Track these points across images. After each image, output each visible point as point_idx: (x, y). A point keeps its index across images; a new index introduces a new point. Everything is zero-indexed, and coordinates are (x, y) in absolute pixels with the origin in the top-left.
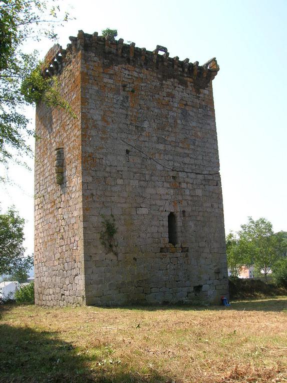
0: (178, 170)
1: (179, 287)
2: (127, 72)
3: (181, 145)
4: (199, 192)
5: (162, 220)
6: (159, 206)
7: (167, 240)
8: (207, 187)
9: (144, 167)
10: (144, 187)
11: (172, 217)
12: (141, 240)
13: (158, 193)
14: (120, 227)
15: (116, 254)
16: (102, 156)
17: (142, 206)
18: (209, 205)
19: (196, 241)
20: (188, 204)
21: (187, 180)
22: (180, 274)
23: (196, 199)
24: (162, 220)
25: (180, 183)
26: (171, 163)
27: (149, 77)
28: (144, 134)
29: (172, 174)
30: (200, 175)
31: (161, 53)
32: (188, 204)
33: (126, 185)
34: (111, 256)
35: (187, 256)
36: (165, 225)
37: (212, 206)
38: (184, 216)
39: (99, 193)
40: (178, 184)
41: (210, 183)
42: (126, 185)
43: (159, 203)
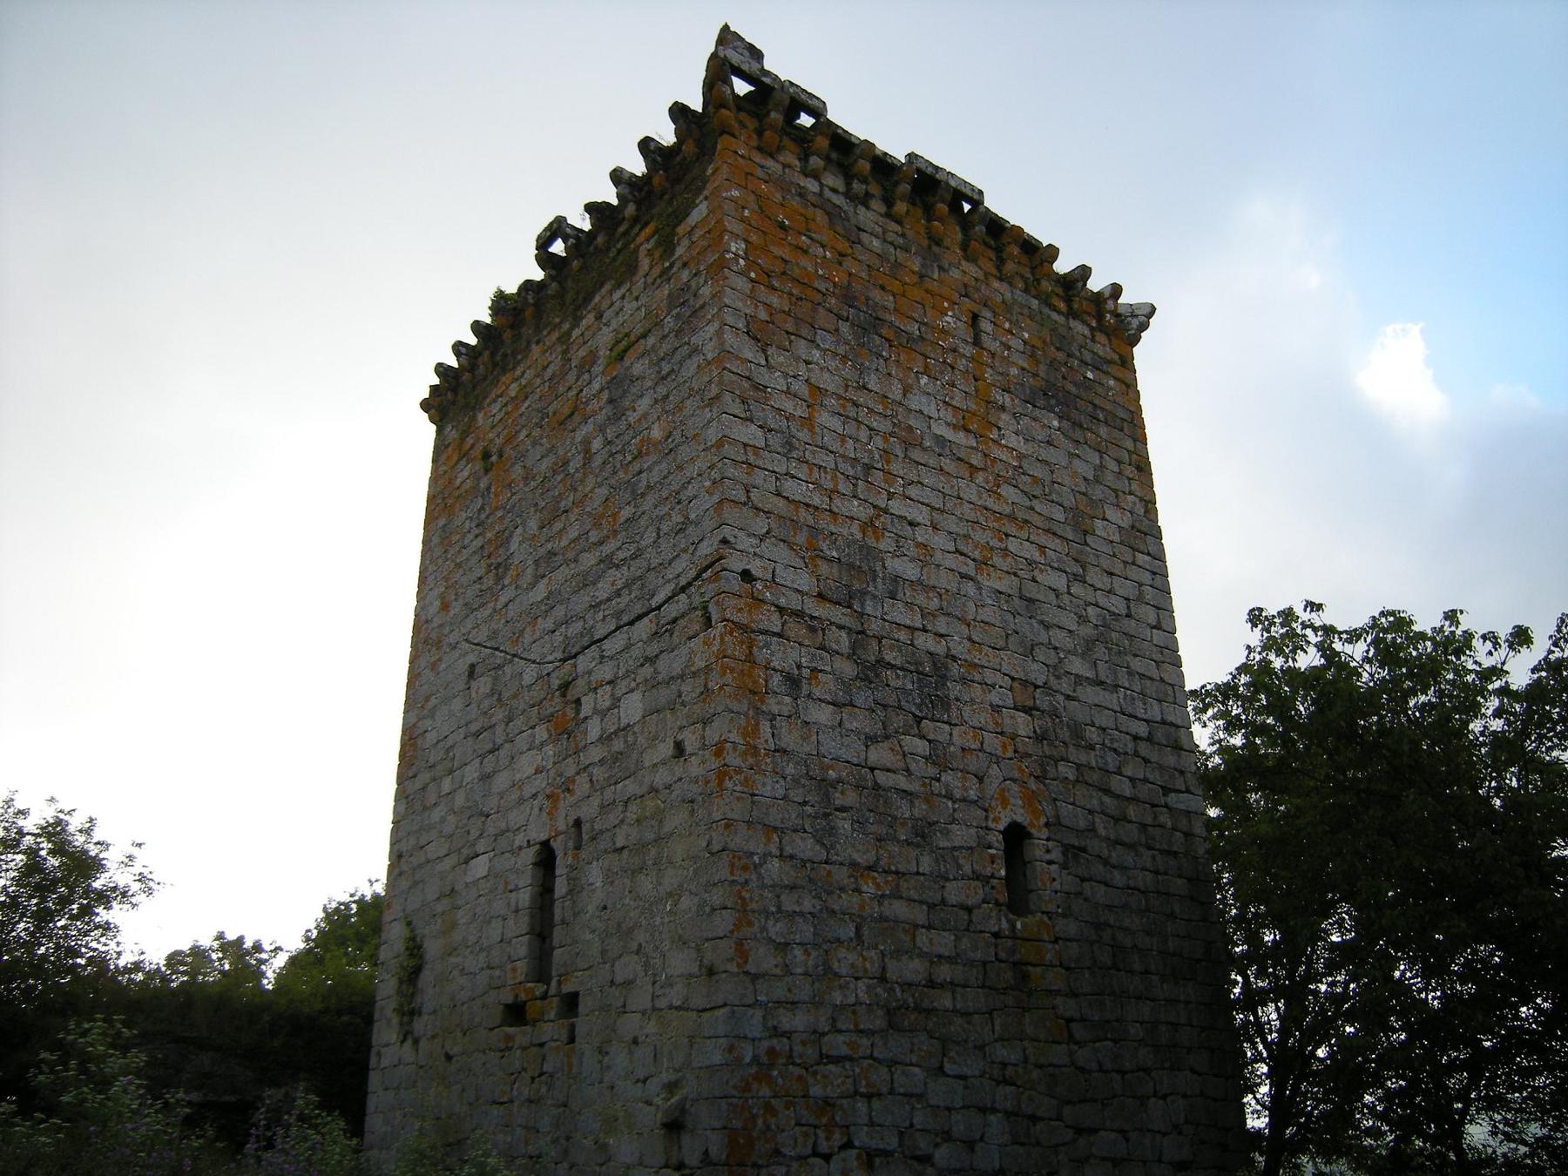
11: (546, 859)
18: (666, 749)
23: (618, 745)
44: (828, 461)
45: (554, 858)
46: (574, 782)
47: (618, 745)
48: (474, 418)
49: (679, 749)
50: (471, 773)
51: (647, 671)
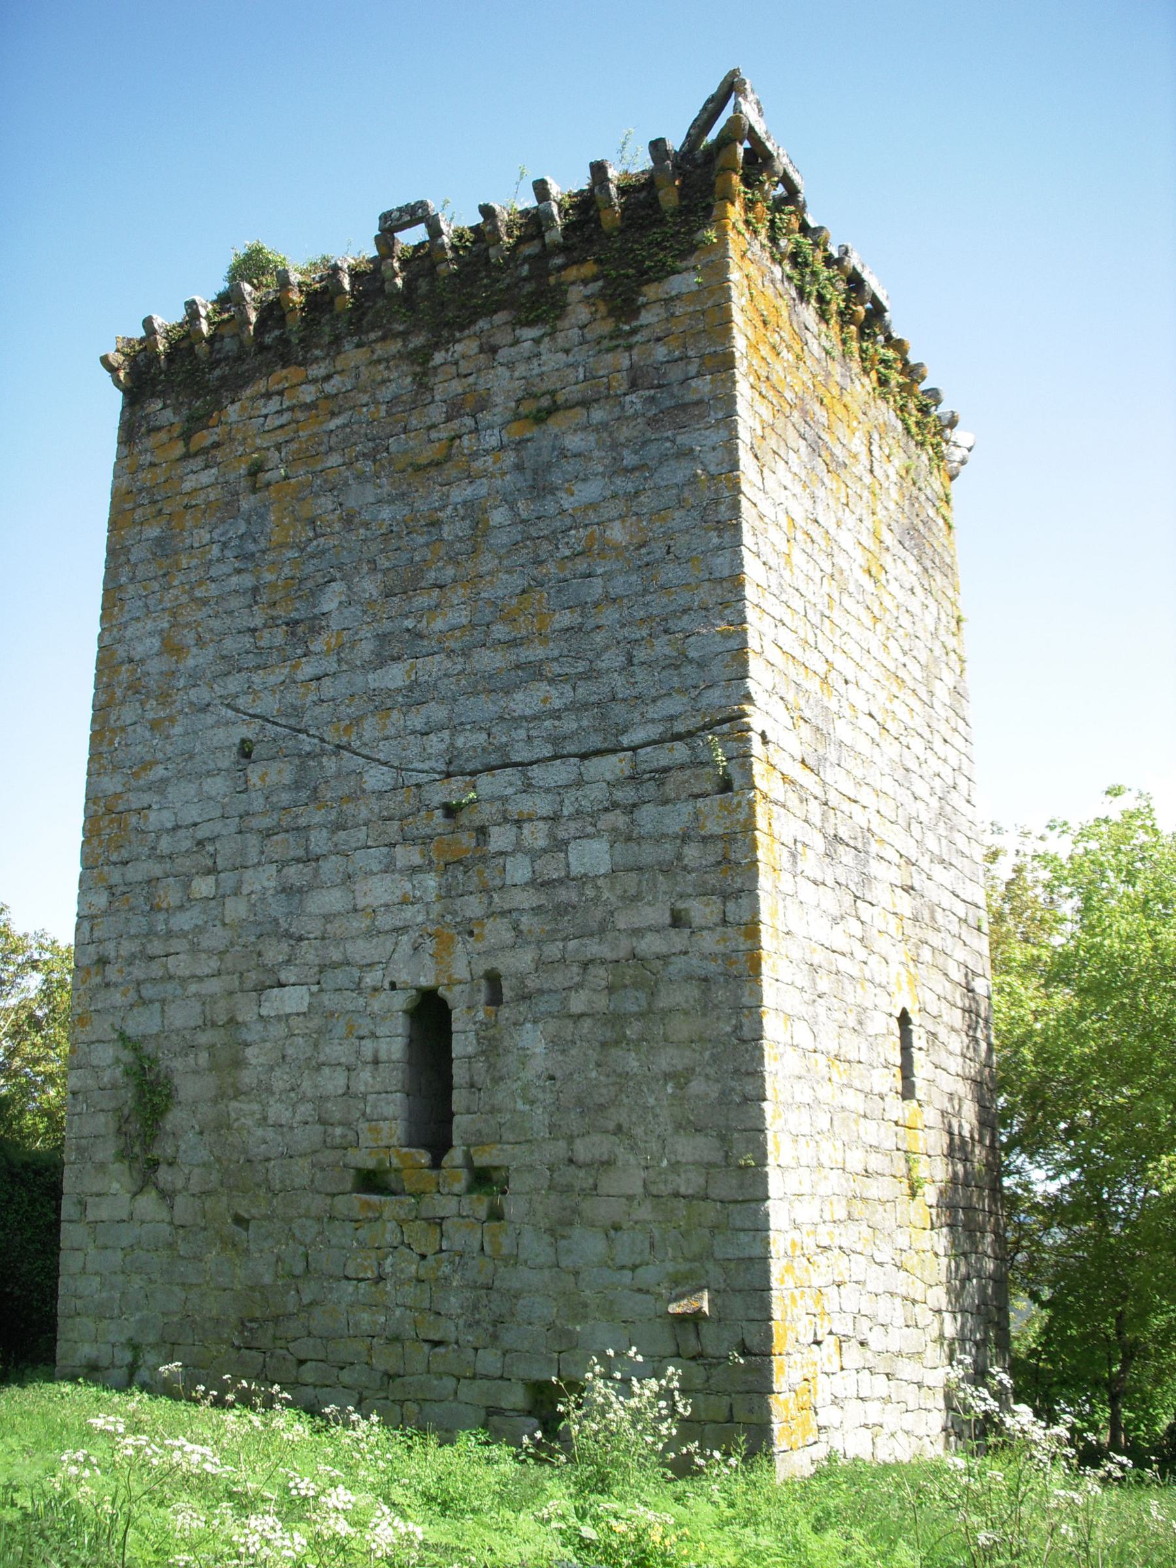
0: (470, 767)
1: (440, 1376)
2: (274, 405)
3: (500, 631)
4: (592, 856)
5: (374, 1036)
6: (361, 967)
7: (394, 1130)
8: (647, 814)
9: (304, 795)
10: (300, 890)
11: (430, 1015)
12: (270, 1134)
13: (362, 902)
14: (192, 1085)
15: (166, 1195)
16: (146, 799)
17: (283, 977)
18: (658, 914)
19: (552, 1127)
20: (519, 932)
21: (525, 804)
22: (453, 1303)
23: (565, 895)
24: (374, 1036)
25: (482, 832)
26: (436, 744)
27: (363, 370)
28: (317, 646)
29: (439, 794)
30: (613, 759)
31: (411, 237)
32: (519, 932)
33: (223, 896)
34: (148, 1203)
35: (496, 1215)
36: (383, 1056)
37: (678, 920)
38: (496, 999)
39: (128, 947)
40: (467, 840)
41: (669, 790)
42: (223, 896)
43: (361, 950)
44: (871, 665)
45: (448, 1013)
46: (483, 925)
47: (565, 895)
48: (219, 406)
49: (678, 920)
50: (263, 880)
51: (618, 819)
